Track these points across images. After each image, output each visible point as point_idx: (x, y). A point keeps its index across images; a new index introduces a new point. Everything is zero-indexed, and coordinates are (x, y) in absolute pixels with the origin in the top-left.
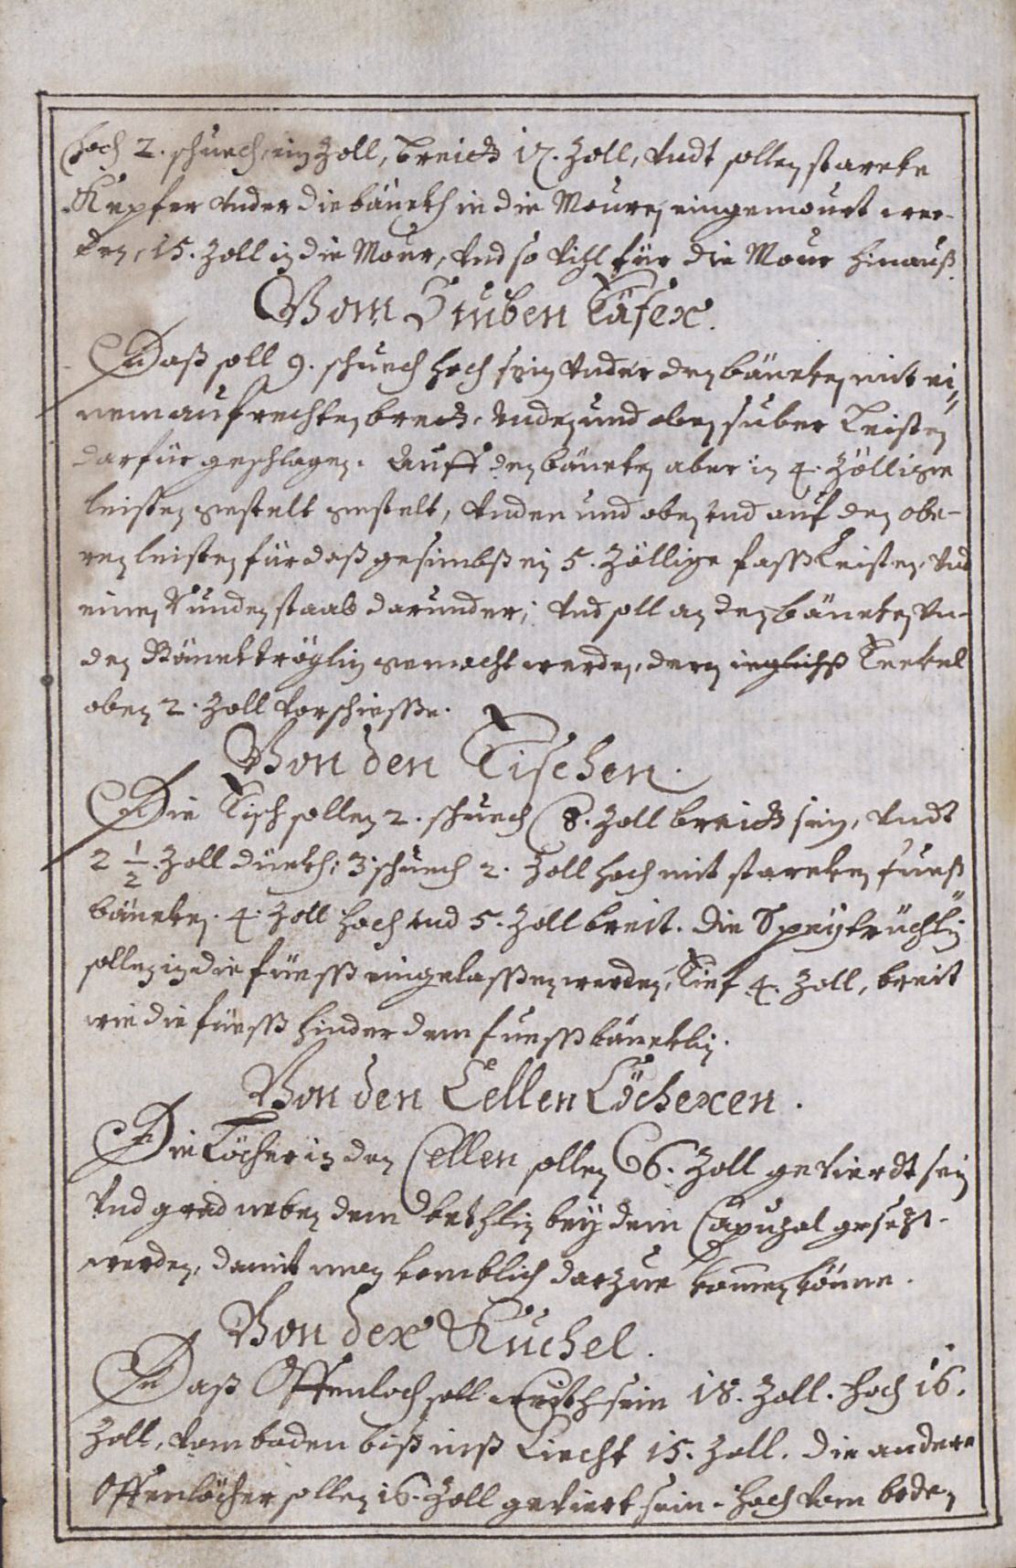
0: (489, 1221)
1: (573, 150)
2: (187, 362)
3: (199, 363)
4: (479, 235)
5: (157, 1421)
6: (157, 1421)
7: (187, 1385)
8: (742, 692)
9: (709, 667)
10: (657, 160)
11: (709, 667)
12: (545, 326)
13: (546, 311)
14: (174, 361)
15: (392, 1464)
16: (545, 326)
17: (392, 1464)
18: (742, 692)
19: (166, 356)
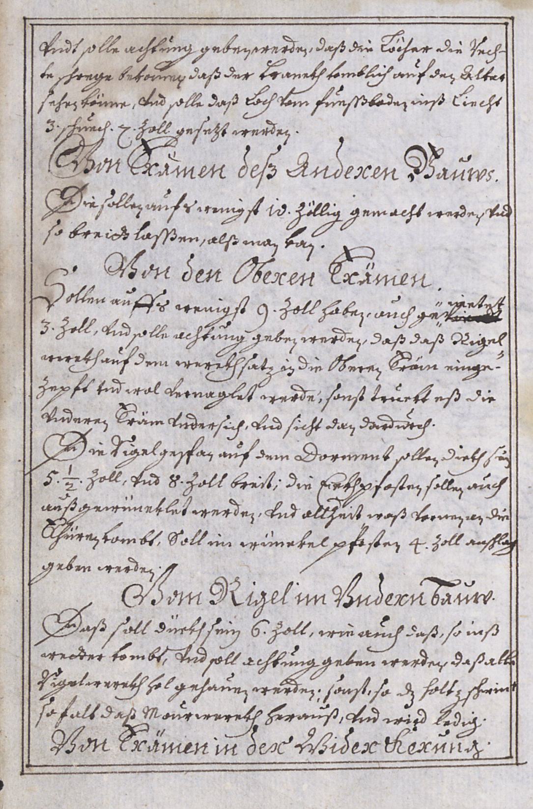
0: (327, 312)
1: (92, 475)
2: (95, 628)
3: (102, 630)
4: (237, 35)
5: (462, 535)
6: (462, 535)
7: (107, 633)
8: (119, 525)
9: (371, 368)
10: (136, 483)
11: (371, 368)
12: (301, 284)
13: (303, 276)
14: (88, 629)
15: (342, 65)
16: (301, 284)
17: (342, 65)
18: (119, 525)
19: (84, 626)
